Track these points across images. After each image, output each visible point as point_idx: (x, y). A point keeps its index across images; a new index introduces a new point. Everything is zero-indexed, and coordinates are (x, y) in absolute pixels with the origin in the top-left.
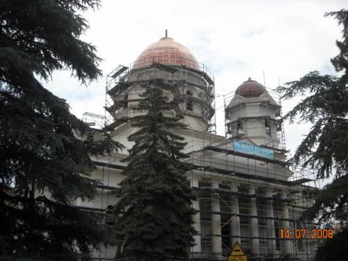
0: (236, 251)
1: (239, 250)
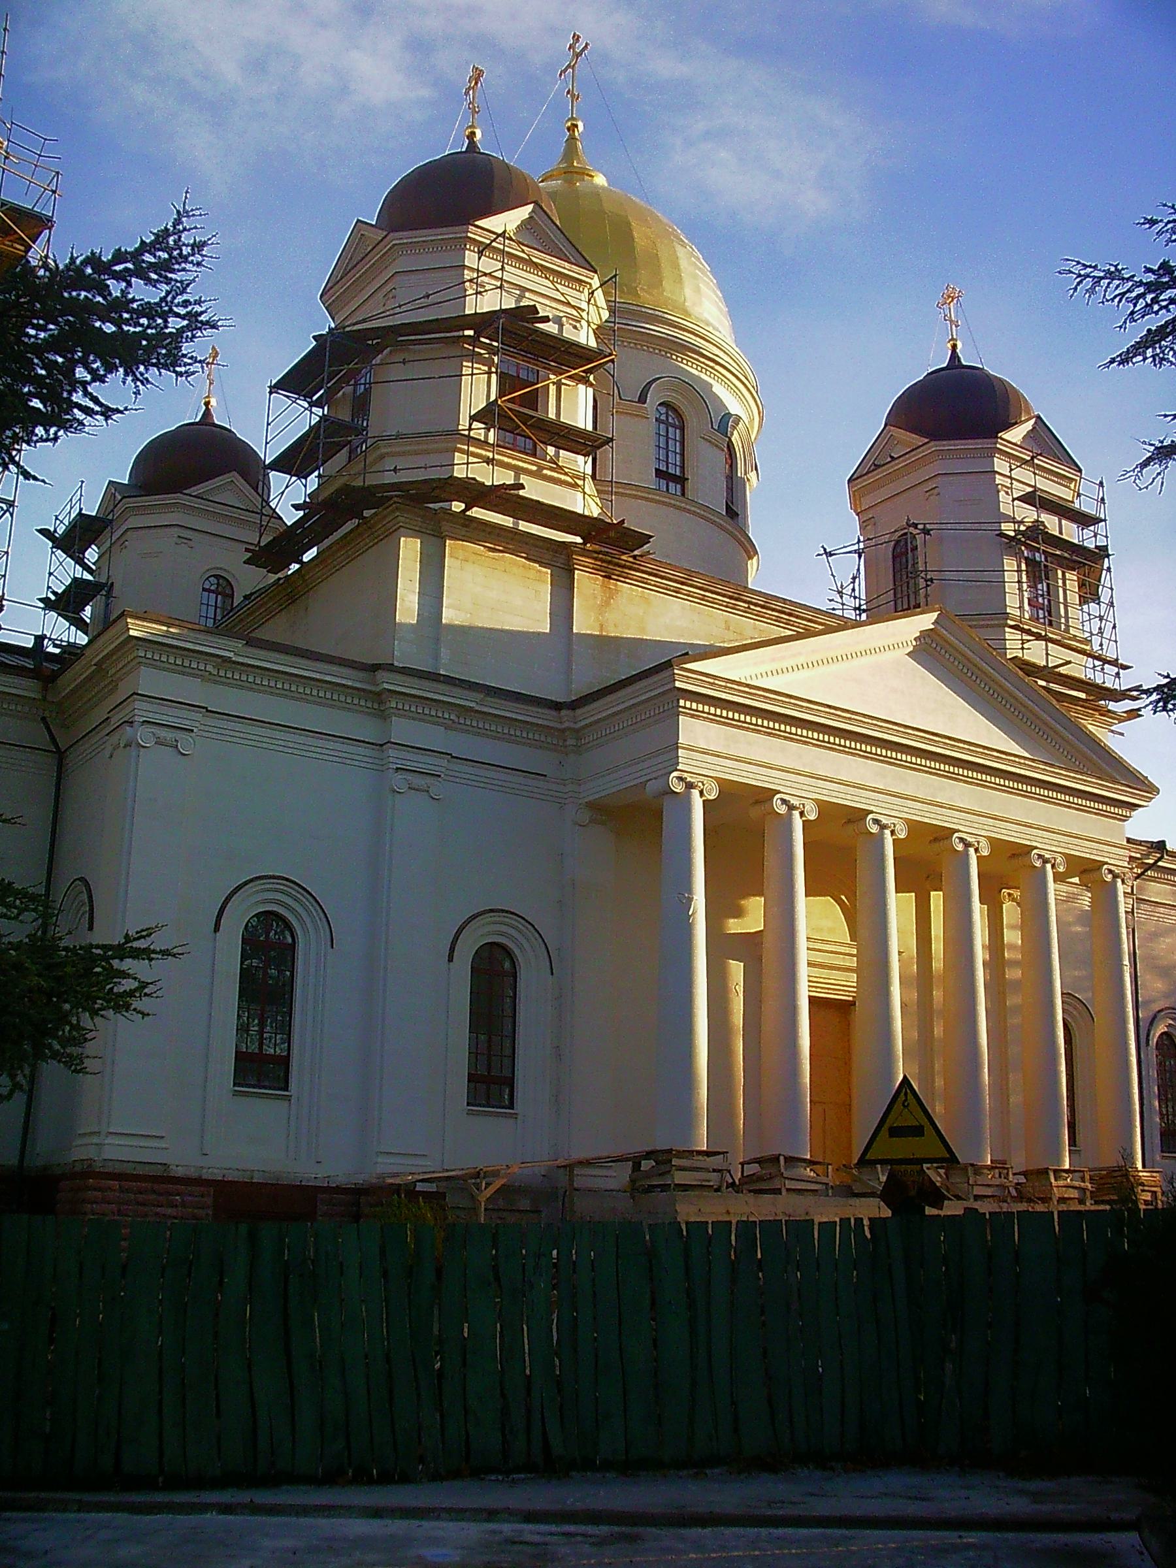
0: (895, 1132)
1: (918, 1131)
